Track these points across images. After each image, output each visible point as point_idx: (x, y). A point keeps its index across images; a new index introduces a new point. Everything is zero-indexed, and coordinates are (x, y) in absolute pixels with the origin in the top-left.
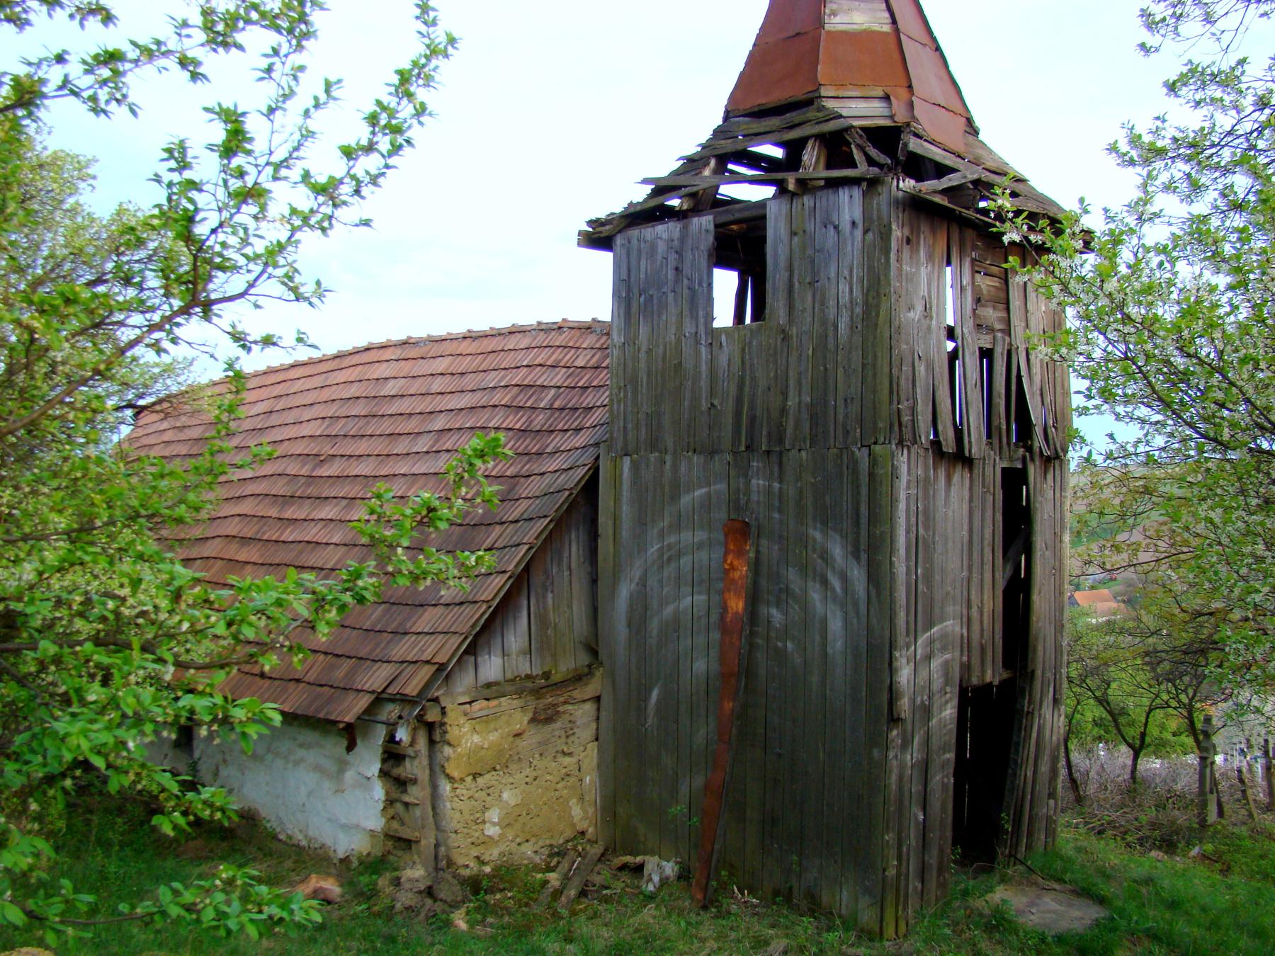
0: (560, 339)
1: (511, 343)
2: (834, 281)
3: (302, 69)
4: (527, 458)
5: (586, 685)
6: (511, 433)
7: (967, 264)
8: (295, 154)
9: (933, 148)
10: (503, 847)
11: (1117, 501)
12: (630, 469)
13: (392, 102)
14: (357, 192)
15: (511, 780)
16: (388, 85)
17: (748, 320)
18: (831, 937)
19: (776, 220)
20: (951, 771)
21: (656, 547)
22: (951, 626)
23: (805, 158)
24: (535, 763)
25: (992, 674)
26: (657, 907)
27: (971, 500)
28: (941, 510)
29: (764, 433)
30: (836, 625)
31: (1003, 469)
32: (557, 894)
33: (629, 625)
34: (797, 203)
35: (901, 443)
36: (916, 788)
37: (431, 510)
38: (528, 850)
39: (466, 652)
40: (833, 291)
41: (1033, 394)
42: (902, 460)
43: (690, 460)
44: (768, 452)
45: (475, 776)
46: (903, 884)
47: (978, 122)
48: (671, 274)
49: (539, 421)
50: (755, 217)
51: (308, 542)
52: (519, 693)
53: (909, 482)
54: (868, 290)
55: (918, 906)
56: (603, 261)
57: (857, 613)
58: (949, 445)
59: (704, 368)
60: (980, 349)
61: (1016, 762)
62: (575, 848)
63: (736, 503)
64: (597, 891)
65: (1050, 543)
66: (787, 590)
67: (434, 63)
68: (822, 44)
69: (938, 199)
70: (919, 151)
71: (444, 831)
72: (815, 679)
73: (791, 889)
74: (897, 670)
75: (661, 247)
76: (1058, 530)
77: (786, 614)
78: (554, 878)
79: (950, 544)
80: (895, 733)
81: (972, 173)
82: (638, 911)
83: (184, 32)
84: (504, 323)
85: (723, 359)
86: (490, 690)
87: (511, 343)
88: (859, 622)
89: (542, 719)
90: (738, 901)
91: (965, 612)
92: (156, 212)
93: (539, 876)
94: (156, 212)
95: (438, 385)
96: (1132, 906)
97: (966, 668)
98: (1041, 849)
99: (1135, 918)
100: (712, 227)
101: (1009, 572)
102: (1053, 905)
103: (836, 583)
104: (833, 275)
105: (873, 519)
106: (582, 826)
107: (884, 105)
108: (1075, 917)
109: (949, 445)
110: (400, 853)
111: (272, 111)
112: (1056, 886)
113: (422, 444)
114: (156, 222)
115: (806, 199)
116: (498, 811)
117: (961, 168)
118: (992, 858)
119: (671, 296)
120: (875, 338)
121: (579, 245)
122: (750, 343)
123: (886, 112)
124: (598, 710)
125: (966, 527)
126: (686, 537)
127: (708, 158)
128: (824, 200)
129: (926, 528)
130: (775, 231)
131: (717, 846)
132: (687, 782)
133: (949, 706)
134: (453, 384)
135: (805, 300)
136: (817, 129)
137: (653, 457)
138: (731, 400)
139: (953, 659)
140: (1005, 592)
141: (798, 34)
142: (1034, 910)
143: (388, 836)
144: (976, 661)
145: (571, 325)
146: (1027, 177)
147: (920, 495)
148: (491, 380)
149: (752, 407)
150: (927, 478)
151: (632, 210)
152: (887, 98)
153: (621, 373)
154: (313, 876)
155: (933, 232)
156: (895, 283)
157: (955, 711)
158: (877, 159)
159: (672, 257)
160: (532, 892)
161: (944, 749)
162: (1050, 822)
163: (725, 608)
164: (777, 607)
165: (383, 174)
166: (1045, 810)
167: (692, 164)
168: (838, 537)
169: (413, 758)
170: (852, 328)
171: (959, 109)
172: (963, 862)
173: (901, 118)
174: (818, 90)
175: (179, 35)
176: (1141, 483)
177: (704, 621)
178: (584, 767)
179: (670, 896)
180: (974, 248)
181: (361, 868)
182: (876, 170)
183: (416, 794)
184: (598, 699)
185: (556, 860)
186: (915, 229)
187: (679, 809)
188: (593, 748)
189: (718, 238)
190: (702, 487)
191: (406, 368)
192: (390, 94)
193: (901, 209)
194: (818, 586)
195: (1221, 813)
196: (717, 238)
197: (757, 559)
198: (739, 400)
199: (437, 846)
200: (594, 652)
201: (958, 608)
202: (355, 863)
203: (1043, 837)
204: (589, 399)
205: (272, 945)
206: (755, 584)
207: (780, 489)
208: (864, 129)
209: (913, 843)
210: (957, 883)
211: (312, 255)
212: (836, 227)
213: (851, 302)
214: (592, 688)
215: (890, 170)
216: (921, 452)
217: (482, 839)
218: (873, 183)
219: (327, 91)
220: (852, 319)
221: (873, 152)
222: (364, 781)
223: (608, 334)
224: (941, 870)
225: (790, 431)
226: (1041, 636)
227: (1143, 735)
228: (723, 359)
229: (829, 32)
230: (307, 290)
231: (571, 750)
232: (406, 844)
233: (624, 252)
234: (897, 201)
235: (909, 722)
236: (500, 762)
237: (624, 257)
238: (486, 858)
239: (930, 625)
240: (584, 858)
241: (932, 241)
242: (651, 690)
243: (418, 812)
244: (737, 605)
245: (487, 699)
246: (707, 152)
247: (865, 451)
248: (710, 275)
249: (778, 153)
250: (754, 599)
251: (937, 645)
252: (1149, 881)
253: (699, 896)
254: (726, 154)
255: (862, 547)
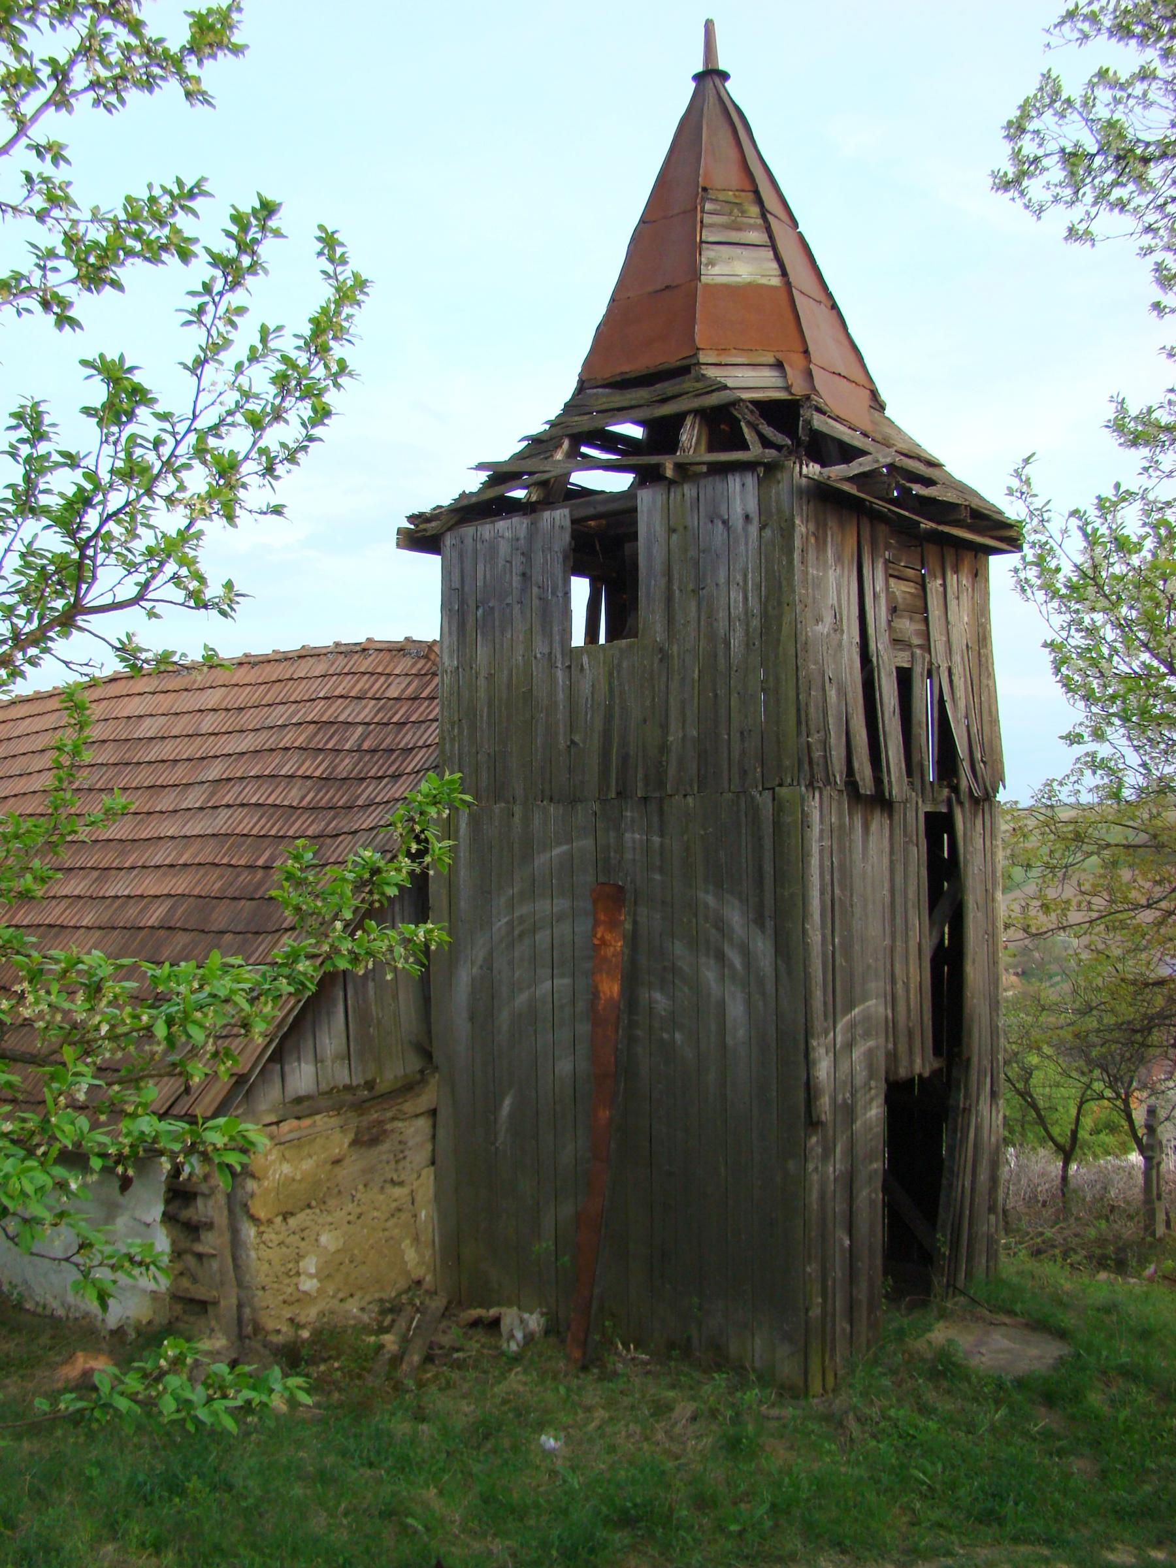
0: (365, 665)
1: (302, 669)
2: (723, 588)
3: (241, 311)
5: (419, 1095)
6: (309, 783)
7: (880, 566)
9: (838, 425)
11: (1045, 850)
14: (270, 470)
15: (330, 1219)
18: (752, 1395)
20: (879, 1184)
21: (505, 920)
22: (874, 1006)
23: (684, 438)
24: (358, 1195)
25: (921, 1063)
26: (525, 1371)
27: (892, 853)
28: (858, 865)
29: (640, 776)
30: (736, 1010)
31: (927, 814)
32: (396, 1360)
33: (472, 1018)
34: (675, 494)
35: (811, 785)
36: (840, 1207)
37: (376, 871)
38: (353, 1306)
40: (723, 601)
41: (958, 722)
42: (814, 805)
45: (286, 1216)
46: (829, 1325)
47: (884, 395)
48: (516, 581)
49: (345, 766)
50: (620, 511)
51: (51, 926)
52: (338, 1108)
53: (822, 831)
54: (767, 597)
56: (430, 566)
57: (763, 994)
59: (561, 696)
60: (898, 668)
61: (952, 1171)
62: (411, 1302)
65: (981, 901)
67: (347, 310)
68: (699, 299)
70: (824, 429)
71: (248, 1288)
73: (689, 1339)
74: (815, 1064)
75: (504, 549)
76: (989, 887)
78: (390, 1341)
80: (814, 1139)
82: (503, 1376)
83: (50, 264)
84: (291, 644)
85: (585, 687)
86: (301, 1107)
87: (302, 669)
89: (367, 1139)
90: (624, 1358)
91: (888, 988)
92: (9, 494)
93: (373, 1339)
94: (9, 494)
95: (208, 724)
99: (1104, 1353)
100: (567, 523)
101: (936, 941)
102: (1005, 1343)
103: (735, 958)
105: (780, 878)
106: (418, 1273)
108: (1036, 1356)
110: (192, 1319)
111: (200, 363)
112: (1007, 1320)
113: (194, 798)
115: (686, 487)
116: (314, 1259)
117: (871, 450)
118: (927, 1288)
119: (516, 609)
121: (399, 546)
122: (619, 665)
123: (780, 383)
124: (434, 1126)
125: (887, 885)
126: (543, 907)
127: (561, 438)
128: (710, 488)
129: (843, 888)
133: (874, 1104)
136: (696, 403)
138: (596, 736)
139: (877, 1047)
140: (933, 960)
142: (983, 1350)
143: (176, 1297)
144: (903, 1048)
145: (379, 646)
146: (942, 461)
147: (835, 847)
148: (279, 716)
150: (842, 826)
151: (465, 502)
152: (779, 365)
155: (842, 526)
156: (800, 590)
157: (880, 1110)
158: (773, 439)
159: (518, 560)
162: (992, 1241)
163: (596, 994)
165: (305, 448)
166: (985, 1228)
167: (539, 445)
168: (736, 903)
169: (206, 1196)
170: (748, 645)
171: (861, 379)
172: (895, 1297)
173: (799, 389)
174: (695, 355)
175: (44, 268)
176: (1071, 828)
178: (418, 1199)
180: (888, 547)
182: (772, 453)
183: (210, 1242)
184: (433, 1113)
185: (389, 1318)
186: (821, 526)
187: (545, 1245)
188: (428, 1174)
190: (561, 845)
192: (298, 348)
194: (712, 962)
195: (1168, 1224)
196: (573, 537)
197: (635, 931)
198: (607, 735)
199: (240, 1306)
200: (426, 1054)
201: (881, 984)
202: (133, 1335)
203: (984, 1261)
204: (408, 738)
206: (633, 962)
207: (662, 845)
208: (756, 403)
209: (839, 1275)
211: (221, 550)
212: (725, 523)
213: (746, 613)
214: (427, 1098)
216: (835, 794)
217: (297, 1295)
218: (771, 468)
220: (747, 633)
221: (768, 431)
222: (144, 1228)
223: (426, 657)
224: (871, 1311)
225: (672, 771)
228: (585, 687)
229: (707, 285)
231: (403, 1177)
232: (201, 1307)
233: (455, 555)
234: (800, 491)
235: (830, 1125)
236: (312, 1198)
238: (302, 1319)
239: (850, 1006)
241: (842, 540)
243: (215, 1265)
244: (611, 988)
245: (298, 1118)
246: (558, 431)
247: (767, 795)
248: (567, 584)
249: (635, 431)
250: (631, 980)
251: (859, 1031)
252: (1109, 1309)
253: (577, 1354)
254: (580, 434)
255: (767, 914)
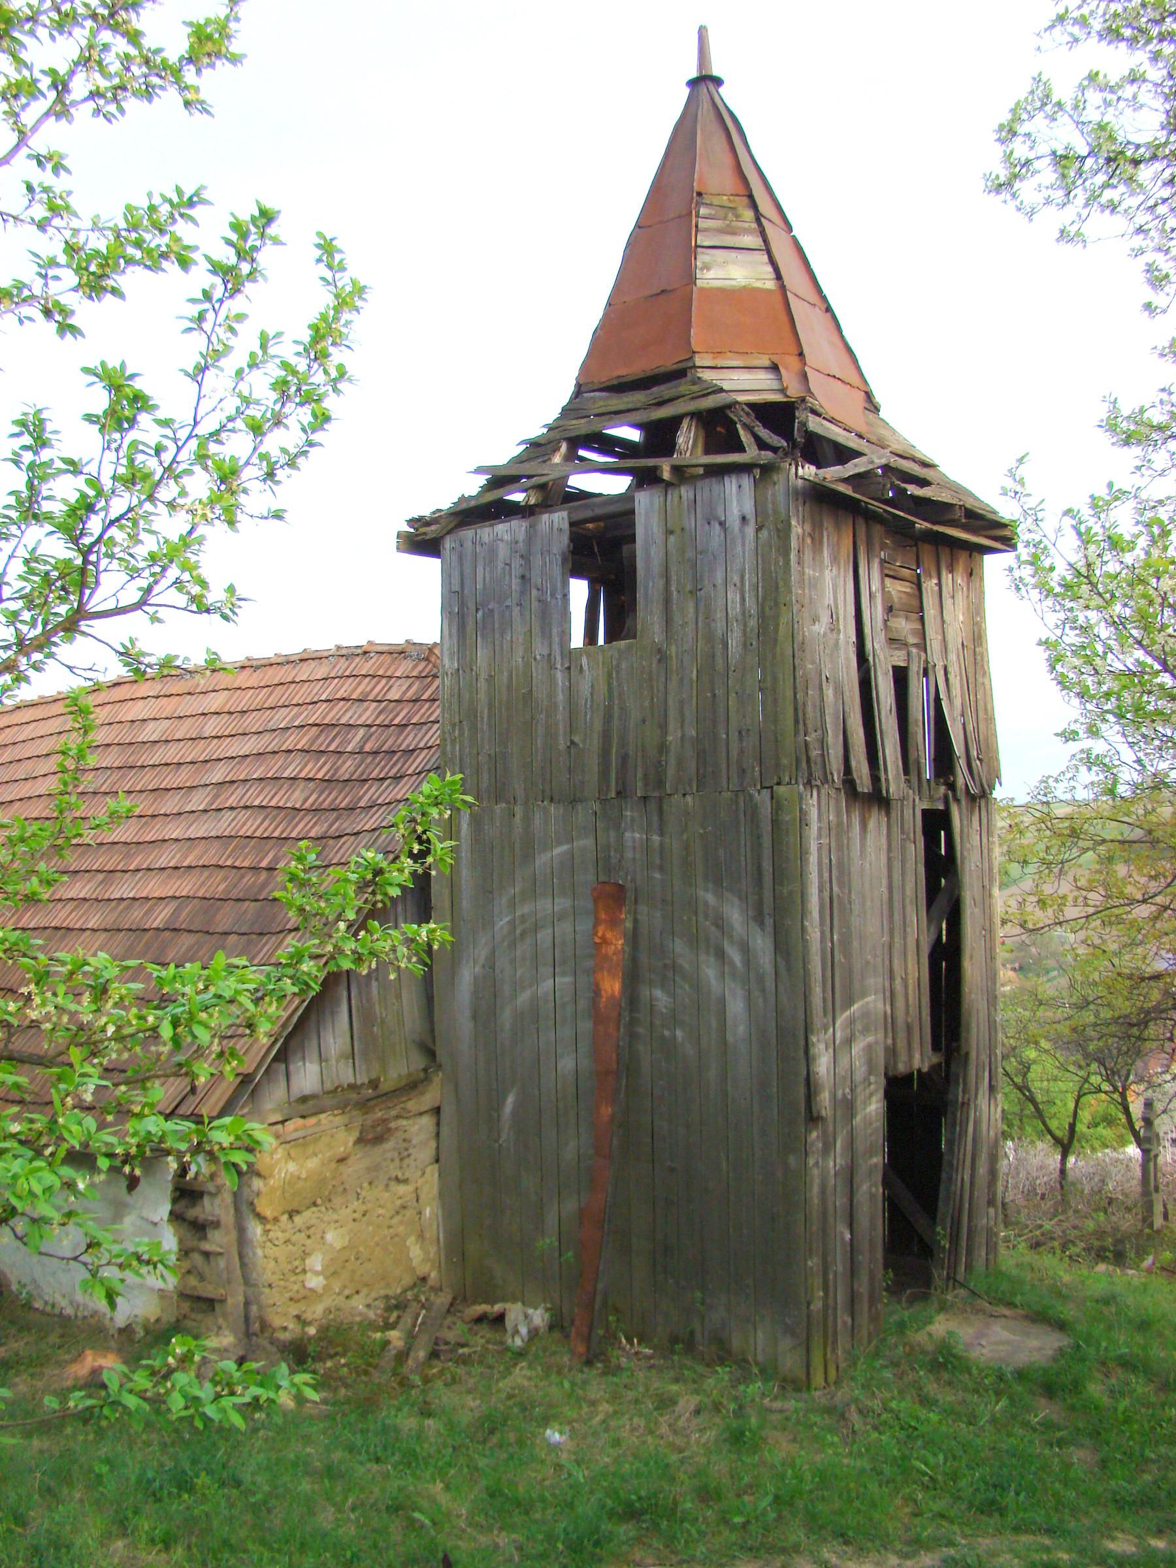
3: (241, 318)
4: (335, 814)
5: (422, 1093)
6: (312, 785)
8: (230, 426)
10: (327, 1302)
12: (470, 824)
13: (302, 365)
14: (270, 475)
15: (335, 1217)
16: (296, 342)
17: (601, 641)
19: (647, 514)
20: (880, 1179)
22: (873, 1002)
24: (363, 1193)
25: (920, 1058)
26: (530, 1367)
27: (889, 849)
29: (639, 775)
30: (736, 1007)
32: (402, 1356)
33: (475, 1017)
34: (673, 495)
36: (841, 1201)
37: (378, 872)
39: (275, 1059)
40: (721, 602)
42: (812, 803)
43: (546, 811)
44: (645, 798)
45: (292, 1214)
47: (878, 397)
48: (515, 583)
49: (347, 768)
51: (56, 928)
52: (343, 1107)
53: (820, 829)
54: (764, 598)
55: (848, 1346)
56: (430, 568)
57: (763, 991)
58: (864, 784)
61: (950, 1164)
63: (604, 862)
64: (452, 1351)
66: (674, 967)
68: (694, 303)
69: (842, 488)
70: (820, 431)
71: (255, 1285)
72: (712, 1074)
73: (692, 1333)
75: (503, 552)
76: (986, 883)
77: (673, 995)
78: (395, 1336)
79: (869, 904)
80: (814, 1134)
81: (880, 458)
82: (508, 1372)
84: (293, 648)
85: (585, 688)
86: (307, 1105)
88: (765, 1001)
89: (371, 1138)
90: (628, 1352)
91: (887, 984)
94: (12, 500)
95: (211, 727)
96: (1098, 1330)
97: (892, 1052)
98: (983, 1269)
99: (1104, 1344)
100: (566, 526)
101: (934, 937)
102: (1006, 1335)
103: (736, 957)
104: (719, 580)
105: (779, 875)
107: (770, 376)
108: (1035, 1347)
109: (864, 784)
110: (199, 1317)
111: (202, 369)
112: (1007, 1312)
113: (198, 801)
114: (14, 514)
115: (683, 490)
117: (866, 451)
118: (927, 1282)
120: (774, 656)
121: (398, 549)
122: (618, 666)
123: (775, 385)
124: (438, 1124)
125: (885, 882)
126: (545, 905)
128: (706, 490)
129: (841, 884)
130: (646, 528)
131: (600, 1286)
132: (556, 1207)
133: (874, 1099)
134: (234, 725)
135: (685, 613)
136: (693, 406)
137: (500, 808)
138: (596, 736)
139: (876, 1043)
141: (663, 291)
142: (984, 1342)
143: (183, 1295)
144: (901, 1044)
145: (380, 649)
146: (936, 462)
147: (833, 845)
148: (281, 718)
149: (623, 744)
150: (839, 824)
151: (464, 506)
152: (775, 368)
153: (455, 707)
154: (89, 1352)
155: (838, 528)
156: (796, 591)
158: (769, 441)
159: (517, 563)
160: (372, 1355)
161: (870, 1152)
162: (991, 1234)
163: (597, 992)
164: (663, 987)
166: (984, 1221)
167: (537, 448)
168: (736, 901)
172: (895, 1290)
173: (794, 391)
175: (45, 277)
176: (1067, 824)
177: (570, 1009)
178: (423, 1196)
179: (545, 1350)
181: (149, 1338)
183: (217, 1241)
184: (437, 1111)
185: (395, 1314)
186: (817, 527)
187: (547, 1242)
188: (433, 1172)
189: (573, 538)
190: (562, 844)
191: (169, 707)
192: (298, 354)
193: (801, 501)
194: (712, 959)
195: (1166, 1216)
197: (635, 929)
198: (606, 736)
199: (247, 1304)
203: (983, 1254)
204: (409, 740)
205: (46, 1444)
206: (634, 959)
207: (662, 844)
208: (751, 405)
209: (840, 1268)
210: (892, 1313)
211: (221, 556)
213: (743, 613)
214: (430, 1096)
215: (786, 454)
216: (833, 793)
217: (303, 1292)
218: (767, 470)
219: (264, 347)
221: (764, 433)
222: (151, 1227)
223: (427, 659)
224: (872, 1301)
225: (671, 772)
226: (974, 1012)
227: (1072, 1127)
228: (585, 688)
229: (702, 289)
230: (215, 595)
232: (209, 1304)
233: (455, 558)
234: (796, 492)
235: (830, 1120)
237: (455, 563)
238: (309, 1316)
239: (849, 1002)
240: (428, 1310)
241: (838, 540)
242: (505, 1099)
243: (222, 1263)
244: (612, 986)
245: (303, 1117)
246: (555, 435)
247: (766, 794)
248: (566, 585)
249: (633, 435)
250: (632, 978)
251: (858, 1026)
253: (581, 1349)
255: (766, 911)
